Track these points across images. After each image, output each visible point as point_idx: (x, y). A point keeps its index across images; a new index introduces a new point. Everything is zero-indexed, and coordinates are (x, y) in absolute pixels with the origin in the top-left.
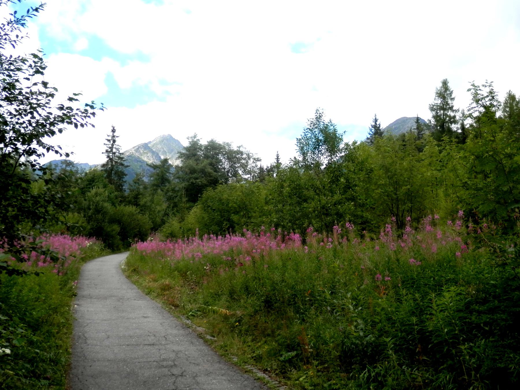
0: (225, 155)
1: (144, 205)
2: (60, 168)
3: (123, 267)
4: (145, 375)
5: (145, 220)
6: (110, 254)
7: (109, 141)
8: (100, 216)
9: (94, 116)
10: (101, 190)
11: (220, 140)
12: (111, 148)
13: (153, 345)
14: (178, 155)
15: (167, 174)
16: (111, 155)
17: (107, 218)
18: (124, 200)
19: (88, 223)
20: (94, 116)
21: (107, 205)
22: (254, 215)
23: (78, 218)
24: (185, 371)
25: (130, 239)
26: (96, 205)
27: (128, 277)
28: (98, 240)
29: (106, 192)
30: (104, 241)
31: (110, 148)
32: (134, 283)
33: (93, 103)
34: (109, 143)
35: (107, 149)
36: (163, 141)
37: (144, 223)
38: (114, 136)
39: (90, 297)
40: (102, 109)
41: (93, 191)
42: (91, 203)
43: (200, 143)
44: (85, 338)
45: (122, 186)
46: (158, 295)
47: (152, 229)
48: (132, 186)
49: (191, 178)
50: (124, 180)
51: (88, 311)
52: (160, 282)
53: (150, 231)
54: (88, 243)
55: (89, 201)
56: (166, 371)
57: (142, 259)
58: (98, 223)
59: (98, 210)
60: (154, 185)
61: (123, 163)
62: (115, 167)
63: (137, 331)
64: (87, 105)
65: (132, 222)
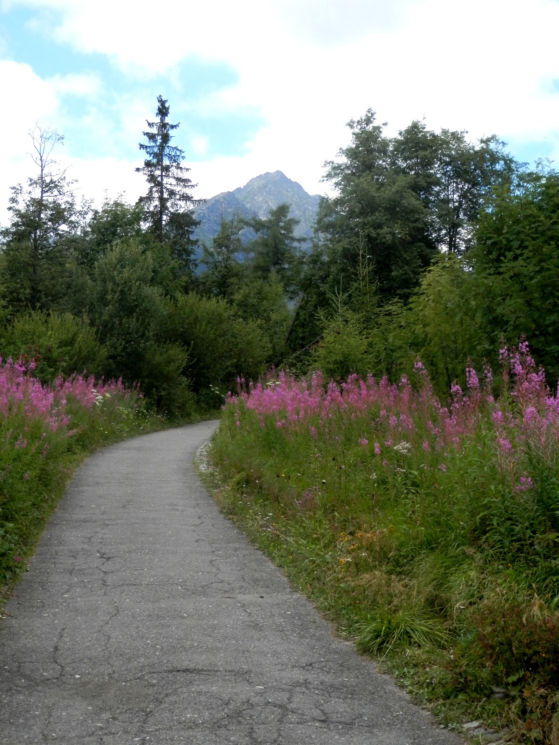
2: (27, 198)
3: (203, 468)
5: (251, 334)
6: (163, 427)
7: (152, 137)
8: (132, 323)
11: (434, 126)
12: (159, 156)
14: (328, 168)
17: (153, 326)
19: (102, 341)
21: (153, 292)
23: (74, 329)
26: (122, 292)
27: (231, 512)
29: (149, 254)
30: (147, 394)
34: (152, 144)
36: (265, 186)
37: (249, 343)
38: (163, 125)
42: (110, 285)
43: (383, 135)
45: (189, 253)
47: (269, 360)
48: (212, 254)
54: (98, 396)
55: (104, 281)
58: (128, 342)
59: (129, 306)
61: (189, 191)
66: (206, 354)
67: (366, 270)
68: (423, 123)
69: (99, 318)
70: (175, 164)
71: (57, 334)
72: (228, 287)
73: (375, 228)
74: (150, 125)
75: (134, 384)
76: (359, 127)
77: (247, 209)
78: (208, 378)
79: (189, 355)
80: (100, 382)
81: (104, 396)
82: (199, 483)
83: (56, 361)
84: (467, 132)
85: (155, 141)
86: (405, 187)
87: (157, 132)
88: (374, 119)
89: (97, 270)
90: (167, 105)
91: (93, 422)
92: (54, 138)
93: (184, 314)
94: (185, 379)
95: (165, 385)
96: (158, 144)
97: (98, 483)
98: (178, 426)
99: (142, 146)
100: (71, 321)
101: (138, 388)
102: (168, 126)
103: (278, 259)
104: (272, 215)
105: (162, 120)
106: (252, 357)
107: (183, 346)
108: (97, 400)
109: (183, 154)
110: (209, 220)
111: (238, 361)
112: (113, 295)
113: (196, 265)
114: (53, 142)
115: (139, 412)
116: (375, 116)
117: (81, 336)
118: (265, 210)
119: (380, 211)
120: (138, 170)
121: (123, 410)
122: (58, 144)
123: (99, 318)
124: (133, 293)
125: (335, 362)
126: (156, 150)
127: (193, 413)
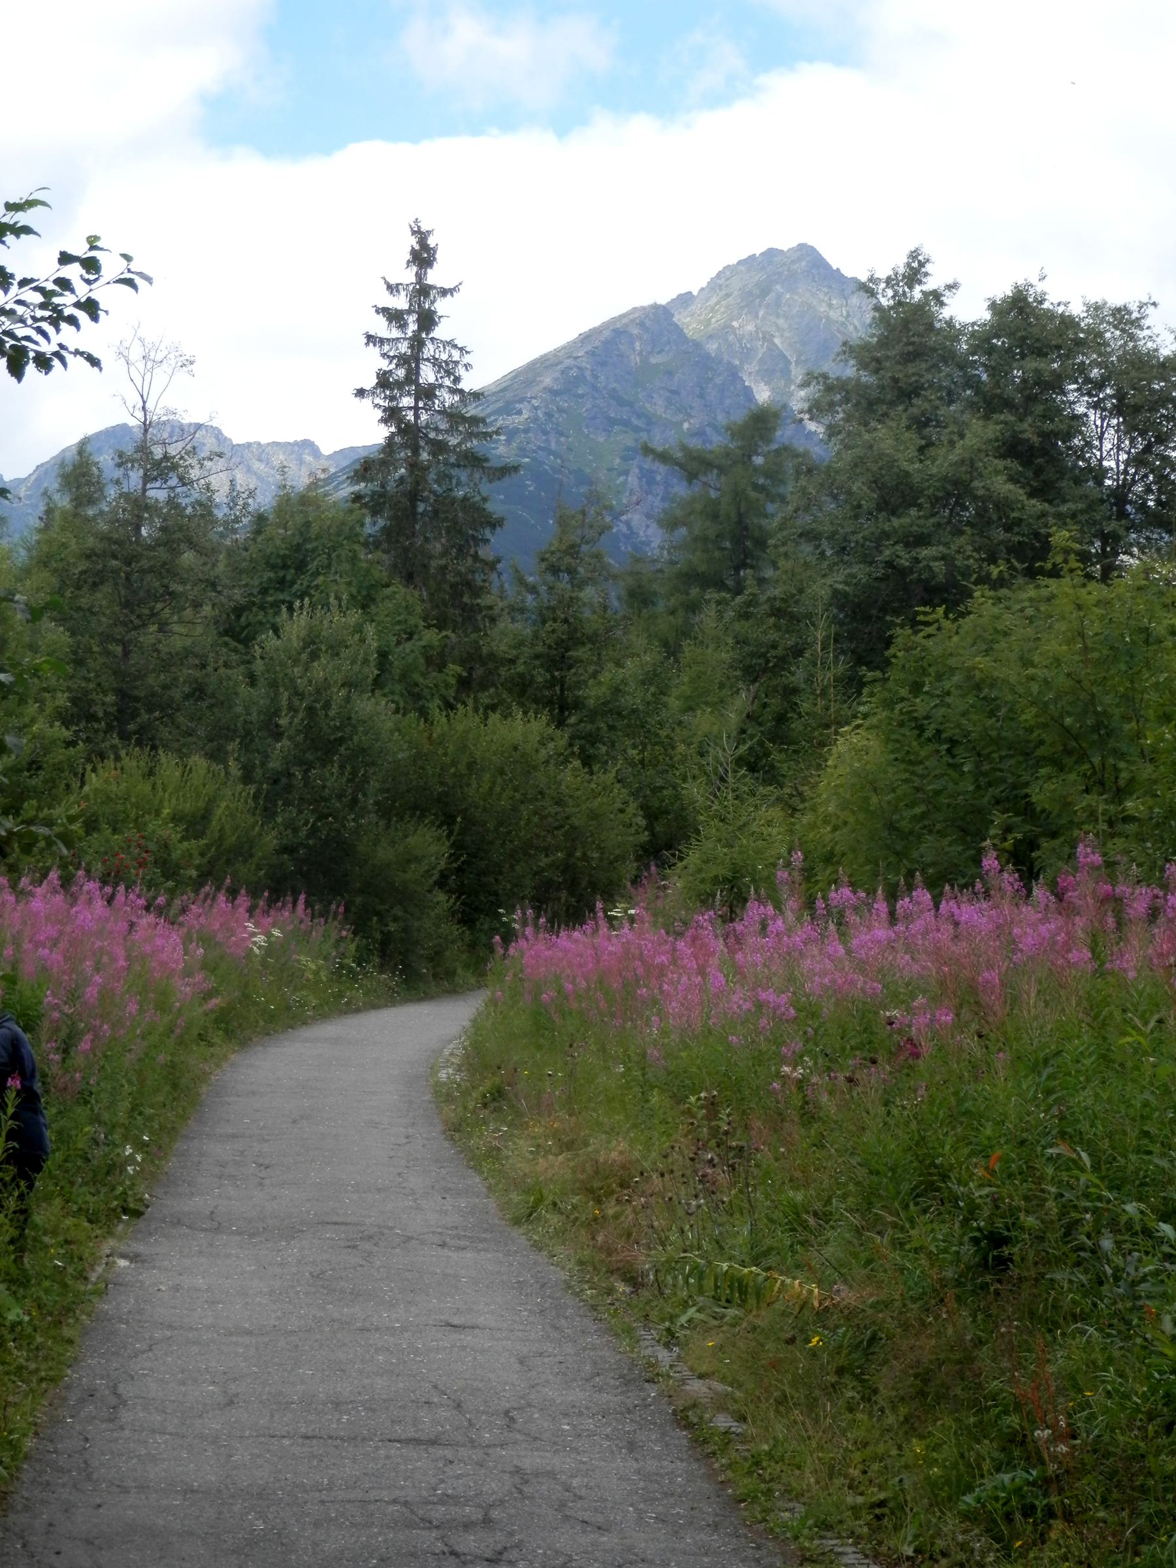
0: (1100, 385)
1: (610, 709)
4: (326, 1547)
5: (601, 797)
6: (392, 998)
7: (394, 317)
8: (331, 777)
9: (95, 318)
10: (339, 620)
11: (1068, 293)
12: (411, 361)
13: (433, 1442)
16: (407, 401)
17: (374, 785)
18: (478, 679)
19: (269, 813)
20: (95, 318)
21: (376, 710)
22: (1146, 771)
24: (519, 1546)
26: (311, 710)
27: (455, 1130)
28: (324, 914)
30: (360, 927)
31: (403, 360)
32: (476, 1160)
33: (93, 248)
34: (395, 333)
35: (385, 365)
37: (594, 816)
38: (422, 291)
39: (216, 1225)
40: (130, 283)
41: (296, 626)
43: (945, 313)
44: (113, 1400)
45: (477, 592)
49: (886, 535)
50: (485, 552)
51: (176, 1288)
53: (630, 868)
54: (257, 935)
55: (274, 685)
56: (427, 1539)
59: (325, 741)
60: (690, 577)
62: (432, 476)
63: (380, 1382)
64: (65, 259)
65: (525, 811)
66: (492, 843)
67: (829, 675)
68: (1039, 290)
69: (263, 764)
70: (447, 382)
71: (174, 801)
72: (570, 667)
73: (907, 545)
74: (392, 289)
75: (333, 907)
76: (890, 293)
77: (707, 357)
78: (496, 894)
79: (451, 846)
80: (261, 903)
81: (268, 935)
82: (428, 1097)
83: (178, 866)
84: (1154, 304)
85: (403, 326)
86: (979, 450)
87: (406, 307)
88: (926, 274)
89: (259, 662)
90: (431, 242)
91: (246, 985)
92: (173, 362)
93: (445, 754)
94: (441, 897)
95: (398, 911)
96: (410, 334)
97: (254, 1093)
98: (426, 997)
99: (370, 339)
100: (202, 772)
101: (340, 917)
102: (433, 293)
103: (747, 554)
105: (420, 277)
106: (600, 848)
107: (439, 827)
108: (255, 943)
109: (467, 359)
110: (594, 388)
111: (570, 855)
112: (292, 718)
113: (493, 620)
114: (170, 371)
115: (342, 966)
116: (928, 268)
117: (223, 805)
118: (762, 362)
119: (920, 507)
120: (361, 393)
121: (308, 963)
122: (181, 375)
123: (263, 764)
124: (332, 713)
126: (404, 348)
127: (459, 971)
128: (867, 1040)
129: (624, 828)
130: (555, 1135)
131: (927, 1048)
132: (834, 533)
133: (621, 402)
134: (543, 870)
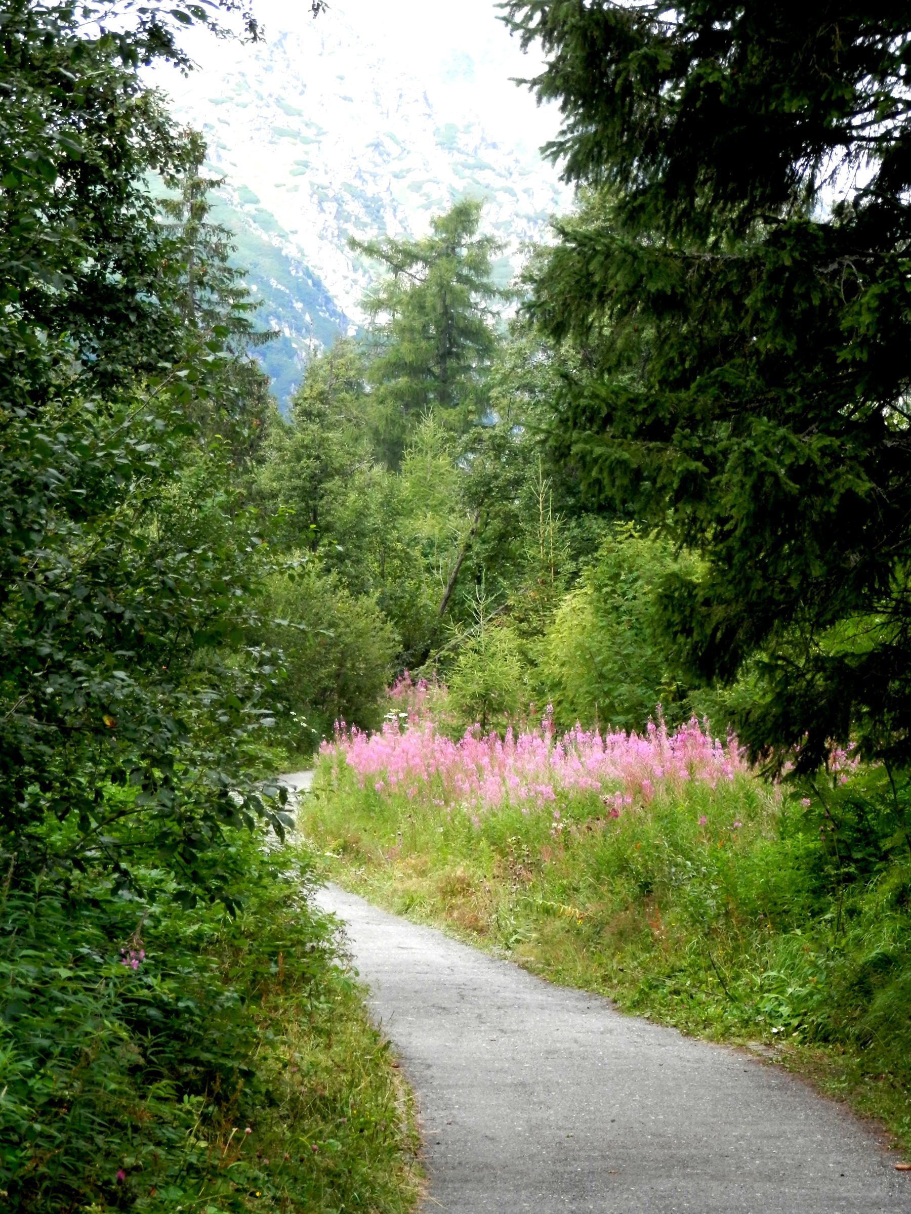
5: (362, 621)
15: (474, 297)
25: (300, 712)
37: (360, 634)
46: (434, 913)
52: (438, 874)
57: (373, 804)
85: (179, 216)
104: (437, 228)
106: (365, 660)
109: (234, 241)
125: (473, 696)
128: (592, 809)
129: (382, 640)
130: (414, 867)
131: (621, 813)
132: (547, 386)
133: (288, 112)
134: (321, 679)
